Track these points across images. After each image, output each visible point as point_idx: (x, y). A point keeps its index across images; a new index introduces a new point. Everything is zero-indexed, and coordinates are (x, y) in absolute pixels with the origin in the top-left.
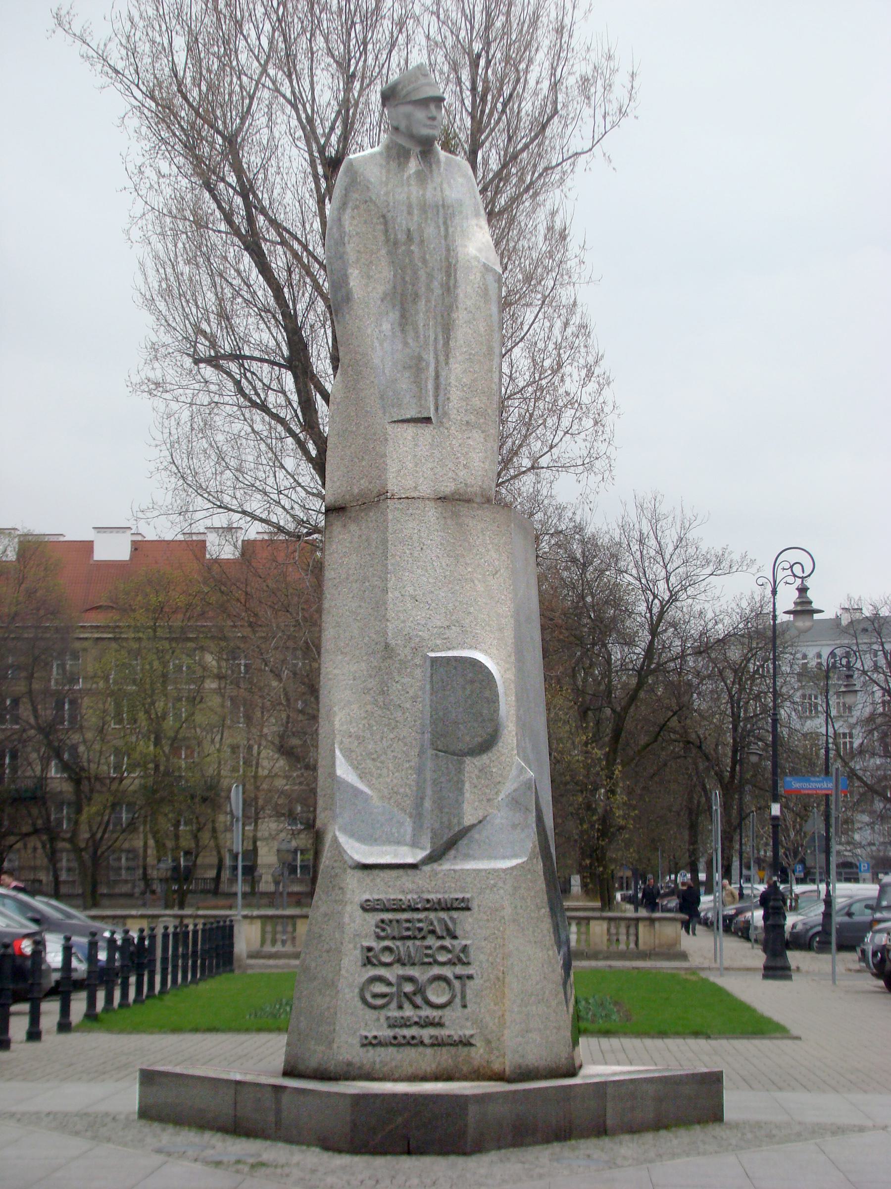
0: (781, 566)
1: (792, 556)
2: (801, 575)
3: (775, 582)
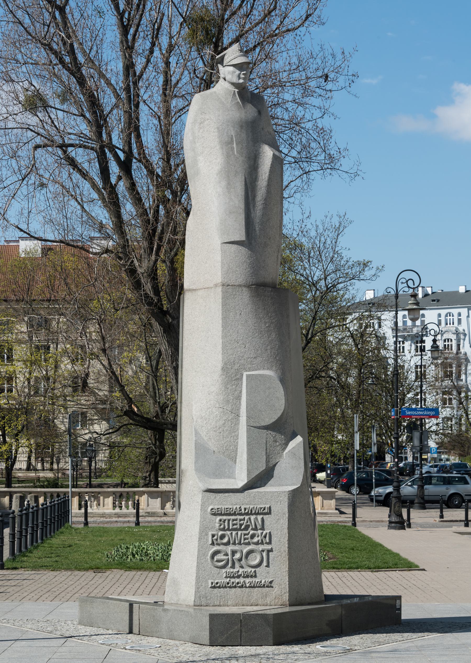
0: (401, 281)
1: (408, 275)
2: (412, 286)
3: (397, 290)
